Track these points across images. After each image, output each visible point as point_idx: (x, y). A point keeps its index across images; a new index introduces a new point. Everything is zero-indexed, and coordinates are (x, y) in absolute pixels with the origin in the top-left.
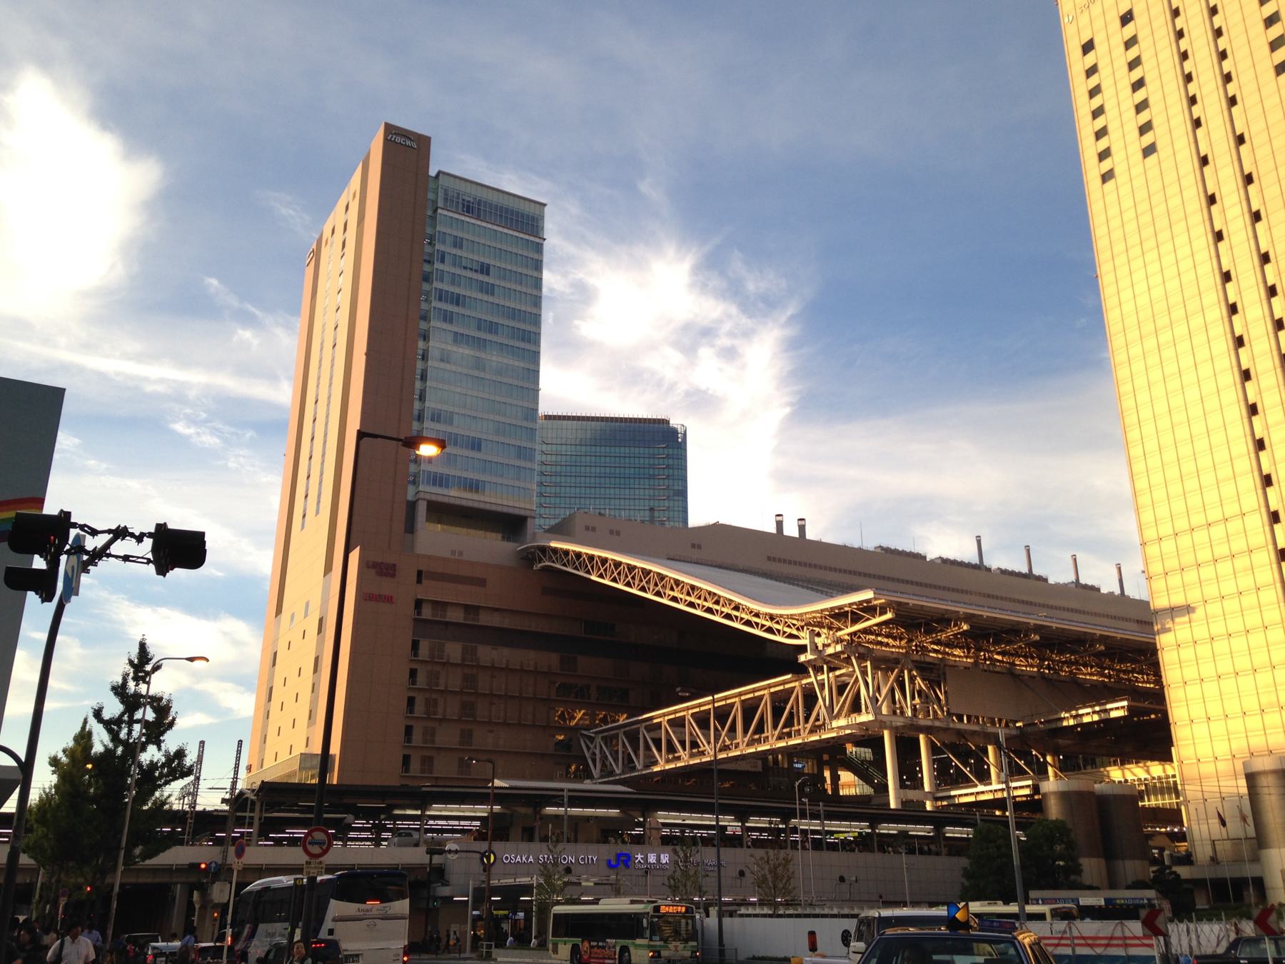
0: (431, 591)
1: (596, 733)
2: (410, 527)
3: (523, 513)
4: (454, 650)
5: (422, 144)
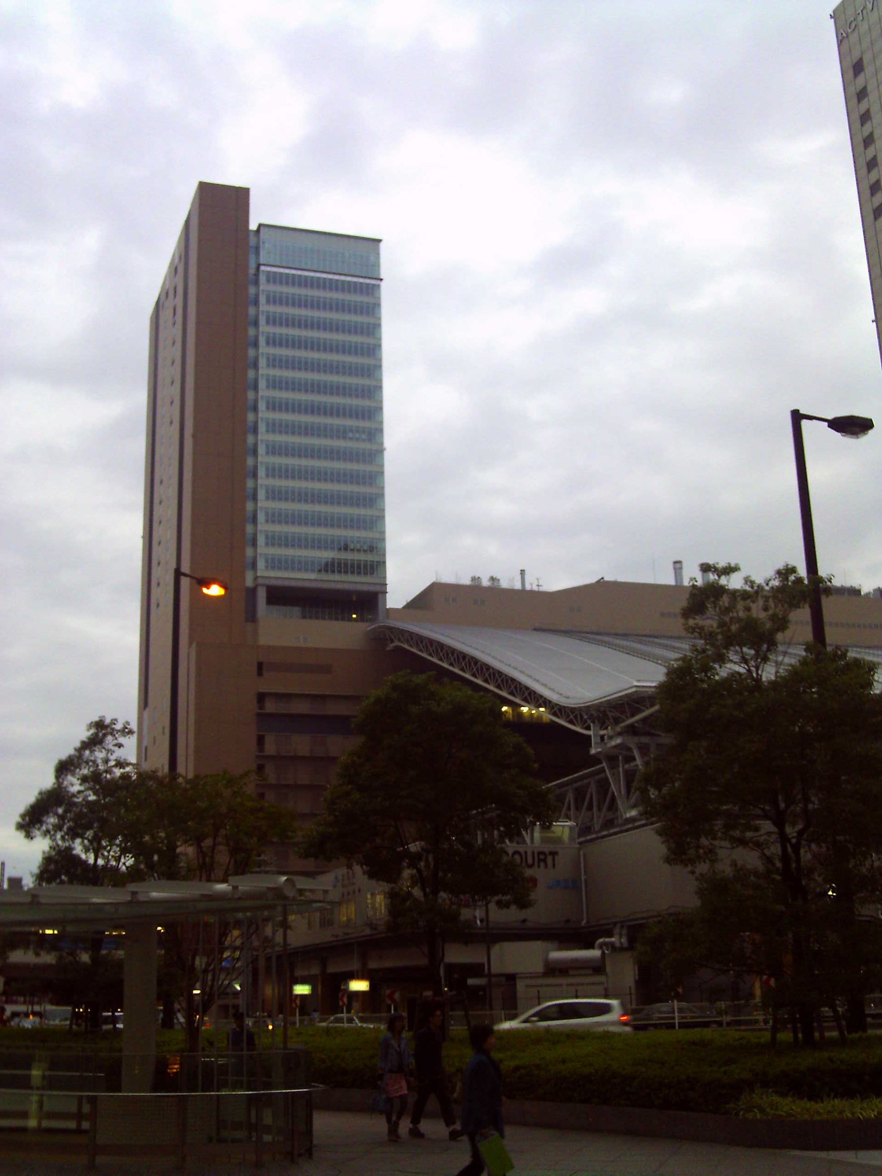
0: (272, 684)
2: (251, 616)
3: (372, 588)
4: (301, 744)
5: (238, 198)
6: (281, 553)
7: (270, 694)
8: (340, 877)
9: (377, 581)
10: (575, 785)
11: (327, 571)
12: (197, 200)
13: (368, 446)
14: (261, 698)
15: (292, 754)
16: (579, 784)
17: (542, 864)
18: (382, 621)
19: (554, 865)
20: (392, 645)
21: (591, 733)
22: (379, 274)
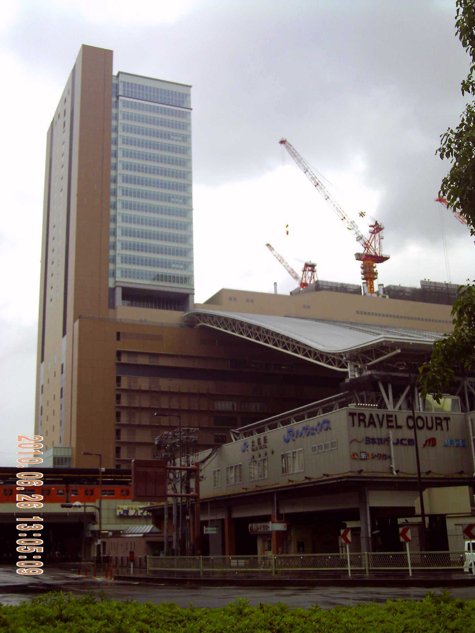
1: (240, 431)
2: (112, 305)
4: (143, 383)
5: (107, 56)
6: (124, 274)
7: (125, 352)
8: (250, 444)
9: (188, 287)
10: (340, 401)
11: (158, 280)
12: (81, 52)
13: (183, 207)
14: (119, 354)
15: (138, 388)
16: (327, 405)
17: (439, 427)
18: (191, 310)
19: (448, 429)
20: (200, 324)
21: (348, 370)
22: (190, 106)
